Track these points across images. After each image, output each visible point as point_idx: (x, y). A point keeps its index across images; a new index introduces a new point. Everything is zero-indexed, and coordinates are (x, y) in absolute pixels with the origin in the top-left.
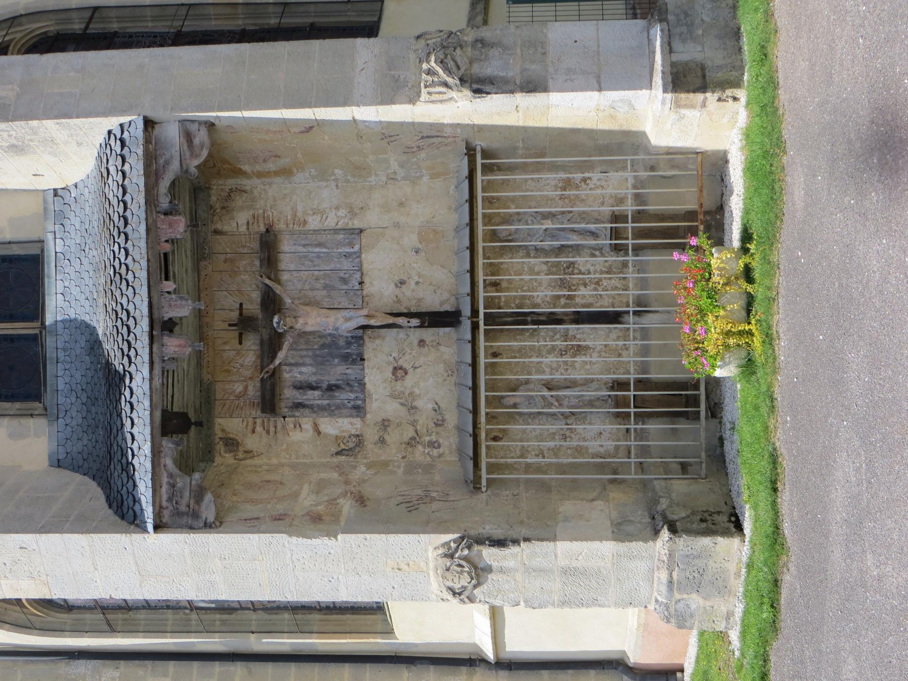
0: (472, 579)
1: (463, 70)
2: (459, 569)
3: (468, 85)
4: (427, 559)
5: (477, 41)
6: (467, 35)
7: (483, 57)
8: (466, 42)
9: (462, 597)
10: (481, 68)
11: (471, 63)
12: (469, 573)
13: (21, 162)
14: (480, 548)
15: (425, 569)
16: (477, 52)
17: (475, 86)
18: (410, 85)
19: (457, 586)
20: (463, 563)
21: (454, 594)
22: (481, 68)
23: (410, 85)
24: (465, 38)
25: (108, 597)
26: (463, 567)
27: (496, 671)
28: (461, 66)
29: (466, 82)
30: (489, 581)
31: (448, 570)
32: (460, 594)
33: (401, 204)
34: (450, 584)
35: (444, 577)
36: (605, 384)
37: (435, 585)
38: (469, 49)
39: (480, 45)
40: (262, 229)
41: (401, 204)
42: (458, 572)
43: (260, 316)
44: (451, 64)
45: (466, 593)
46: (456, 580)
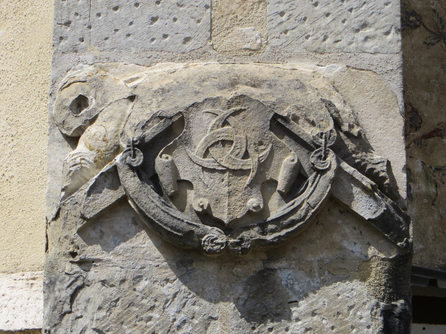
0: (229, 229)
2: (281, 175)
4: (277, 55)
9: (131, 182)
12: (257, 217)
13: (443, 284)
14: (377, 272)
15: (225, 42)
19: (185, 161)
20: (314, 193)
21: (148, 147)
26: (290, 193)
30: (204, 307)
31: (279, 125)
32: (146, 173)
34: (202, 130)
35: (239, 106)
37: (138, 84)
42: (263, 166)
43: (276, 226)
45: (149, 201)
46: (224, 157)
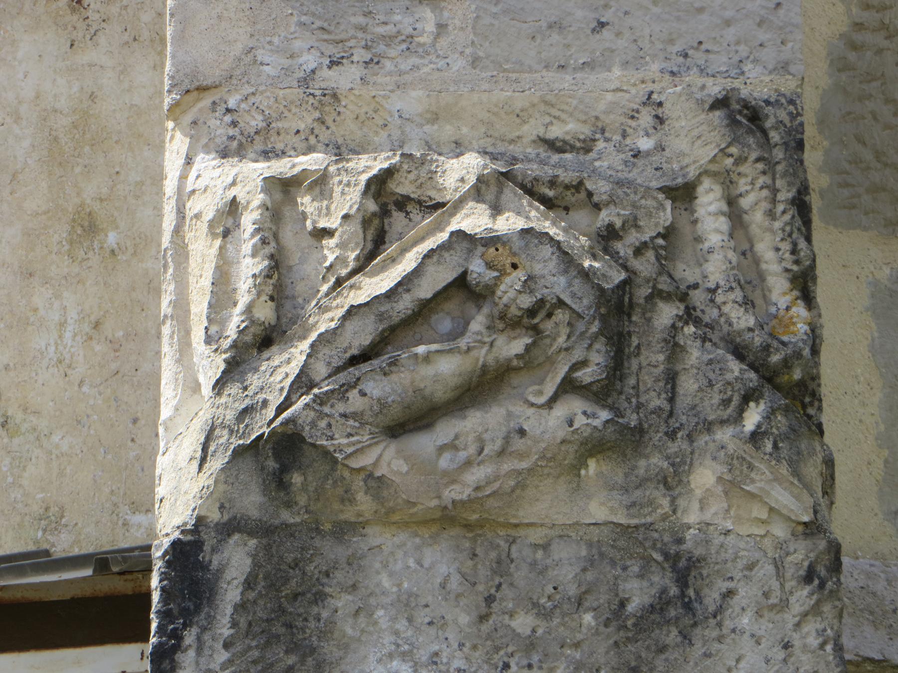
1: (389, 459)
3: (252, 501)
5: (685, 569)
6: (732, 487)
7: (523, 623)
8: (673, 481)
10: (407, 605)
11: (448, 519)
16: (566, 568)
17: (235, 561)
18: (344, 79)
22: (407, 605)
23: (344, 79)
24: (705, 477)
25: (292, 263)
27: (723, 197)
28: (424, 443)
29: (278, 483)
33: (87, 227)
36: (365, 211)
38: (600, 509)
39: (638, 595)
40: (627, 596)
41: (87, 227)
44: (436, 366)
